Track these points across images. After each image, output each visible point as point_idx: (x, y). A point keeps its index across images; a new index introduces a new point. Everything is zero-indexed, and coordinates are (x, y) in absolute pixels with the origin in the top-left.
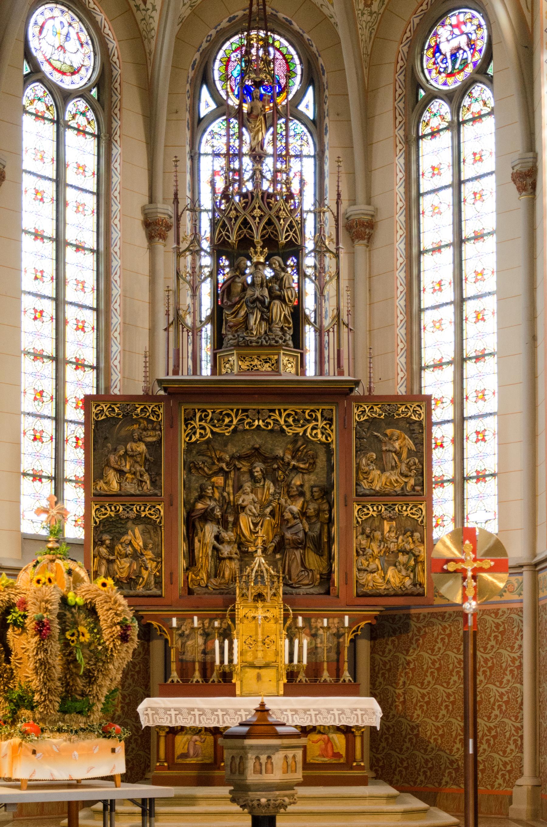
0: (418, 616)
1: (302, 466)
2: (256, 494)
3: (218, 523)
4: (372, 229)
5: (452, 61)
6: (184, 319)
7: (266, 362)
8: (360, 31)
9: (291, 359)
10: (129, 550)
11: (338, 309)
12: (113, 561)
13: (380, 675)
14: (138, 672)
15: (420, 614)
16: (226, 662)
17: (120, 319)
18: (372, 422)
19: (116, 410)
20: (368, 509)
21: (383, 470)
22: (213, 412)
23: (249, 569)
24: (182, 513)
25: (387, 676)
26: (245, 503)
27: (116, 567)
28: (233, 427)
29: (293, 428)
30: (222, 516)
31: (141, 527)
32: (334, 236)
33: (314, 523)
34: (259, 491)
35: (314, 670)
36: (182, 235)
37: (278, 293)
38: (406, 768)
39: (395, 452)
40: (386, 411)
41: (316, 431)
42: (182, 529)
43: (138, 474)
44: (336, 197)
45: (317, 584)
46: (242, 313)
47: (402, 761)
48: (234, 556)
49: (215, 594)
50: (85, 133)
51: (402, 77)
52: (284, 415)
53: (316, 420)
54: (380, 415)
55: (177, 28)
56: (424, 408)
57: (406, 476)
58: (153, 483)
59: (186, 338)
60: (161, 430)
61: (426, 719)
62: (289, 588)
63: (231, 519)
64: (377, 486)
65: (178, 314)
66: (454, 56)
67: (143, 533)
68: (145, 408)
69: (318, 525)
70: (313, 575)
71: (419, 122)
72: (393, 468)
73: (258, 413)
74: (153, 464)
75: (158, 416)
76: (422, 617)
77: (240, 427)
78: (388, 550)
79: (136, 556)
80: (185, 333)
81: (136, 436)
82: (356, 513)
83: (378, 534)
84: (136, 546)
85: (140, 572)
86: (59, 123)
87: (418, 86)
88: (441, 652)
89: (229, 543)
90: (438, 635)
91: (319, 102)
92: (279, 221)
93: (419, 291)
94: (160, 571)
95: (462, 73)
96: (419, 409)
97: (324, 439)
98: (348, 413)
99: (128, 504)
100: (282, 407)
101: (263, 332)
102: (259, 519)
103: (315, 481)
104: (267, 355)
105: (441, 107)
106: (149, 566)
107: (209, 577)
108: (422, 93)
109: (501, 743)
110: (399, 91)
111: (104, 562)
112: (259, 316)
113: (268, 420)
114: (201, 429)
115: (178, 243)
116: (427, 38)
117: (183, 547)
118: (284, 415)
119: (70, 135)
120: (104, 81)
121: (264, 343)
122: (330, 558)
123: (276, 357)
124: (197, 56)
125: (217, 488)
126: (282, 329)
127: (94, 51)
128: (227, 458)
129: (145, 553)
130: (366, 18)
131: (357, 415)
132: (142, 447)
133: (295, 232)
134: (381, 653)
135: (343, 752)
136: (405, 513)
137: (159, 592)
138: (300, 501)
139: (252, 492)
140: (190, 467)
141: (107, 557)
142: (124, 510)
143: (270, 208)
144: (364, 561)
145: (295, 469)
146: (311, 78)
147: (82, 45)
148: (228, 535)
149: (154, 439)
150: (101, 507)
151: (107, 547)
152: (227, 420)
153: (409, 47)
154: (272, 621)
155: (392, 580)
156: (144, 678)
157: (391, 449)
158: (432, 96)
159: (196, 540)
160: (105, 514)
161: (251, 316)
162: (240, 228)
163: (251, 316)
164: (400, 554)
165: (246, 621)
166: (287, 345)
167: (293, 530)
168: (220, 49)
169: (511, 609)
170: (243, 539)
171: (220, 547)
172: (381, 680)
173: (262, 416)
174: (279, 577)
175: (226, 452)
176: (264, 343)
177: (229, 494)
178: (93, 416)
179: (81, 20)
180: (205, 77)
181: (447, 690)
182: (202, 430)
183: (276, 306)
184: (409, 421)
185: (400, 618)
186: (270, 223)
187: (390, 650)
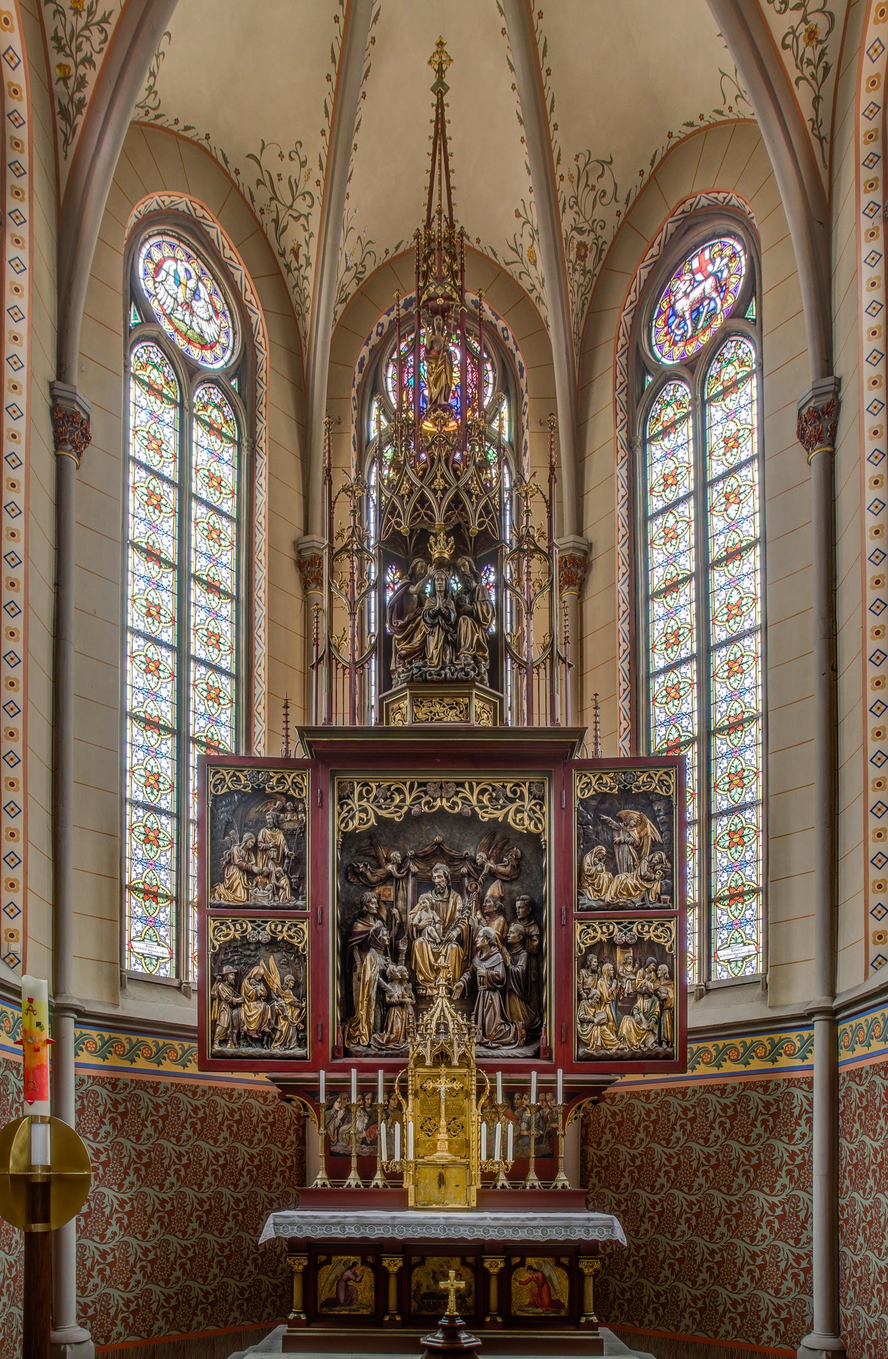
3: (385, 954)
5: (692, 320)
7: (451, 709)
8: (570, 295)
9: (487, 707)
11: (551, 635)
12: (238, 1006)
13: (593, 1175)
14: (290, 1168)
16: (397, 1158)
17: (265, 687)
18: (602, 797)
19: (242, 778)
20: (595, 930)
21: (615, 872)
22: (377, 787)
24: (332, 939)
25: (603, 1175)
28: (406, 808)
29: (490, 810)
30: (391, 943)
32: (545, 529)
33: (518, 953)
35: (517, 1173)
38: (629, 1301)
39: (632, 845)
42: (333, 964)
43: (274, 876)
46: (418, 638)
47: (623, 1291)
48: (408, 1000)
51: (623, 360)
52: (476, 791)
54: (611, 789)
55: (341, 308)
56: (673, 777)
57: (649, 880)
61: (657, 1236)
62: (483, 1049)
63: (403, 947)
66: (696, 310)
67: (279, 966)
68: (283, 777)
73: (441, 788)
74: (294, 866)
77: (415, 810)
80: (340, 671)
82: (578, 936)
86: (183, 406)
88: (681, 1143)
89: (401, 982)
90: (676, 1121)
92: (470, 498)
93: (647, 650)
94: (304, 1022)
96: (667, 778)
97: (532, 828)
98: (568, 786)
104: (453, 697)
106: (289, 1013)
109: (771, 1277)
110: (620, 379)
113: (455, 799)
114: (360, 811)
118: (476, 791)
120: (245, 367)
130: (577, 276)
131: (582, 787)
133: (492, 520)
134: (595, 1145)
135: (565, 1300)
136: (647, 937)
138: (500, 920)
143: (458, 478)
146: (508, 384)
147: (217, 313)
148: (399, 970)
152: (397, 799)
153: (633, 318)
154: (461, 1096)
156: (297, 1175)
158: (666, 377)
160: (228, 935)
162: (415, 509)
165: (421, 1096)
166: (482, 682)
169: (790, 1080)
171: (388, 986)
172: (594, 1180)
173: (448, 792)
178: (211, 788)
179: (215, 278)
181: (689, 1197)
182: (363, 812)
185: (623, 1097)
186: (457, 501)
187: (608, 1141)
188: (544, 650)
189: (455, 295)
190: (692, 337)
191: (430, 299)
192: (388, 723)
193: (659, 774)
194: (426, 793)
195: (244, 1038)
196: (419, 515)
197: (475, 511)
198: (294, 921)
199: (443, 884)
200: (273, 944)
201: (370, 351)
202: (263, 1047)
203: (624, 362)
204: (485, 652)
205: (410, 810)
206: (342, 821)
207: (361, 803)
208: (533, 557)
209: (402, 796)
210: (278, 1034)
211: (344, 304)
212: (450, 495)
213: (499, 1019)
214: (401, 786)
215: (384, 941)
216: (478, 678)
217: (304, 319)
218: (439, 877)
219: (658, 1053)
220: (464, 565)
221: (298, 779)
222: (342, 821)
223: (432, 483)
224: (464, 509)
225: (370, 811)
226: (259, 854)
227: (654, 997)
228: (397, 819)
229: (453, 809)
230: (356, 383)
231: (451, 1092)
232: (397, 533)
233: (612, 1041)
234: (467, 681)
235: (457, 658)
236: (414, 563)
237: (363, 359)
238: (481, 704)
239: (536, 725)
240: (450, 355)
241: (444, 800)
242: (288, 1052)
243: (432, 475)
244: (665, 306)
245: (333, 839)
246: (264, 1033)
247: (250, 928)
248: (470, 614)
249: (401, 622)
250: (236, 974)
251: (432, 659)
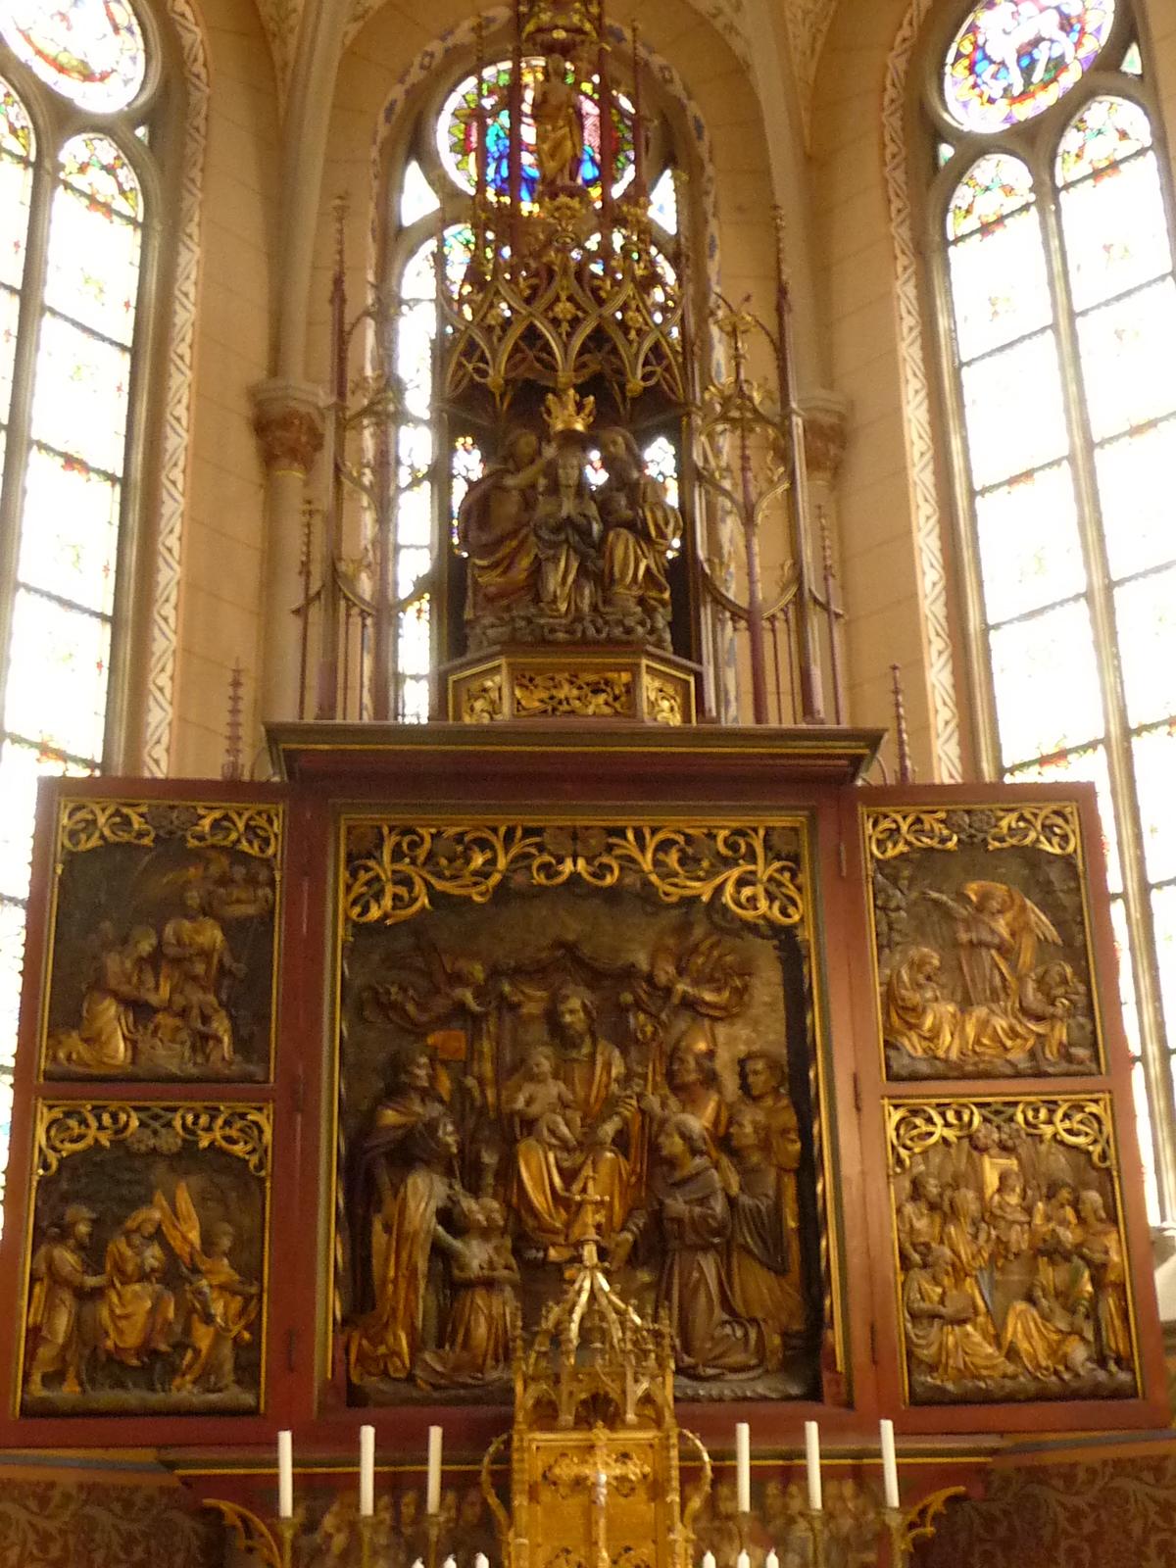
0: (1069, 1475)
1: (709, 997)
2: (568, 1081)
3: (449, 1173)
4: (843, 447)
6: (352, 581)
7: (596, 691)
8: (790, 26)
9: (670, 690)
10: (153, 1256)
12: (98, 1293)
15: (1074, 1465)
18: (925, 861)
23: (556, 1311)
24: (331, 1141)
26: (535, 1109)
27: (105, 1313)
28: (496, 878)
30: (461, 1151)
31: (197, 1181)
34: (578, 1074)
36: (351, 375)
37: (629, 513)
39: (999, 949)
40: (959, 830)
41: (749, 892)
42: (331, 1195)
43: (195, 1012)
44: (773, 298)
45: (772, 1364)
46: (525, 562)
49: (436, 1402)
50: (108, 210)
52: (651, 844)
53: (751, 857)
54: (944, 840)
55: (353, 28)
57: (1039, 1018)
58: (241, 1044)
59: (357, 634)
60: (272, 883)
63: (489, 1158)
64: (949, 1045)
65: (335, 570)
67: (201, 1201)
68: (226, 817)
69: (771, 1176)
70: (760, 1334)
71: (945, 211)
72: (995, 997)
73: (575, 837)
74: (243, 988)
75: (266, 841)
76: (1082, 1475)
77: (519, 879)
78: (1002, 1251)
79: (174, 1274)
80: (356, 620)
81: (193, 898)
83: (968, 1196)
84: (177, 1243)
85: (187, 1330)
87: (938, 132)
89: (485, 1233)
91: (690, 200)
94: (254, 1327)
95: (1053, 87)
96: (1060, 821)
99: (156, 1106)
100: (645, 822)
101: (585, 606)
102: (579, 1157)
103: (748, 1042)
104: (597, 671)
105: (1003, 176)
106: (218, 1308)
107: (416, 1348)
108: (946, 152)
111: (67, 1296)
112: (575, 565)
114: (396, 883)
115: (341, 394)
116: (951, 39)
117: (331, 1250)
118: (651, 844)
119: (64, 206)
121: (591, 631)
122: (1133, 1371)
123: (625, 677)
124: (398, 93)
125: (445, 1063)
126: (641, 601)
127: (147, 51)
128: (478, 972)
129: (204, 1264)
132: (212, 935)
133: (668, 369)
137: (247, 1399)
139: (556, 1076)
140: (363, 1003)
141: (77, 1279)
142: (142, 1124)
144: (927, 1286)
145: (689, 1004)
148: (481, 1209)
149: (251, 910)
150: (68, 1115)
151: (80, 1247)
152: (478, 860)
153: (909, 61)
155: (1024, 1346)
157: (986, 937)
158: (974, 148)
159: (378, 1226)
160: (81, 1137)
161: (549, 567)
163: (550, 566)
164: (1043, 1261)
165: (546, 1495)
166: (659, 644)
167: (694, 1191)
168: (452, 90)
170: (531, 1222)
171: (457, 1244)
174: (657, 1335)
175: (475, 956)
176: (591, 631)
177: (481, 1081)
180: (418, 146)
183: (623, 545)
184: (1031, 857)
188: (784, 589)
189: (588, 26)
190: (1023, 94)
191: (540, 30)
192: (458, 717)
193: (1042, 814)
194: (541, 848)
195: (104, 1365)
196: (524, 360)
197: (637, 355)
198: (240, 1107)
199: (581, 1026)
200: (188, 1157)
201: (407, 92)
202: (152, 1389)
203: (898, 124)
204: (662, 590)
205: (505, 880)
206: (354, 903)
207: (397, 867)
208: (752, 430)
209: (489, 855)
210: (189, 1355)
211: (361, 23)
212: (586, 329)
213: (720, 1315)
214: (487, 834)
215: (448, 1145)
216: (652, 639)
217: (284, 42)
218: (572, 1012)
219: (1098, 1385)
220: (615, 443)
221: (262, 822)
222: (354, 903)
223: (550, 307)
224: (615, 351)
225: (417, 880)
226: (165, 970)
227: (1076, 1259)
228: (477, 899)
229: (602, 877)
230: (379, 140)
231: (621, 1485)
232: (483, 389)
233: (989, 1357)
234: (628, 643)
235: (607, 601)
236: (512, 437)
237: (393, 103)
238: (657, 684)
239: (773, 723)
240: (580, 116)
241: (581, 862)
242: (213, 1397)
243: (550, 295)
244: (967, 48)
245: (337, 934)
246: (155, 1353)
247: (977, 1120)
248: (630, 525)
249: (485, 538)
250: (95, 1222)
251: (554, 601)
